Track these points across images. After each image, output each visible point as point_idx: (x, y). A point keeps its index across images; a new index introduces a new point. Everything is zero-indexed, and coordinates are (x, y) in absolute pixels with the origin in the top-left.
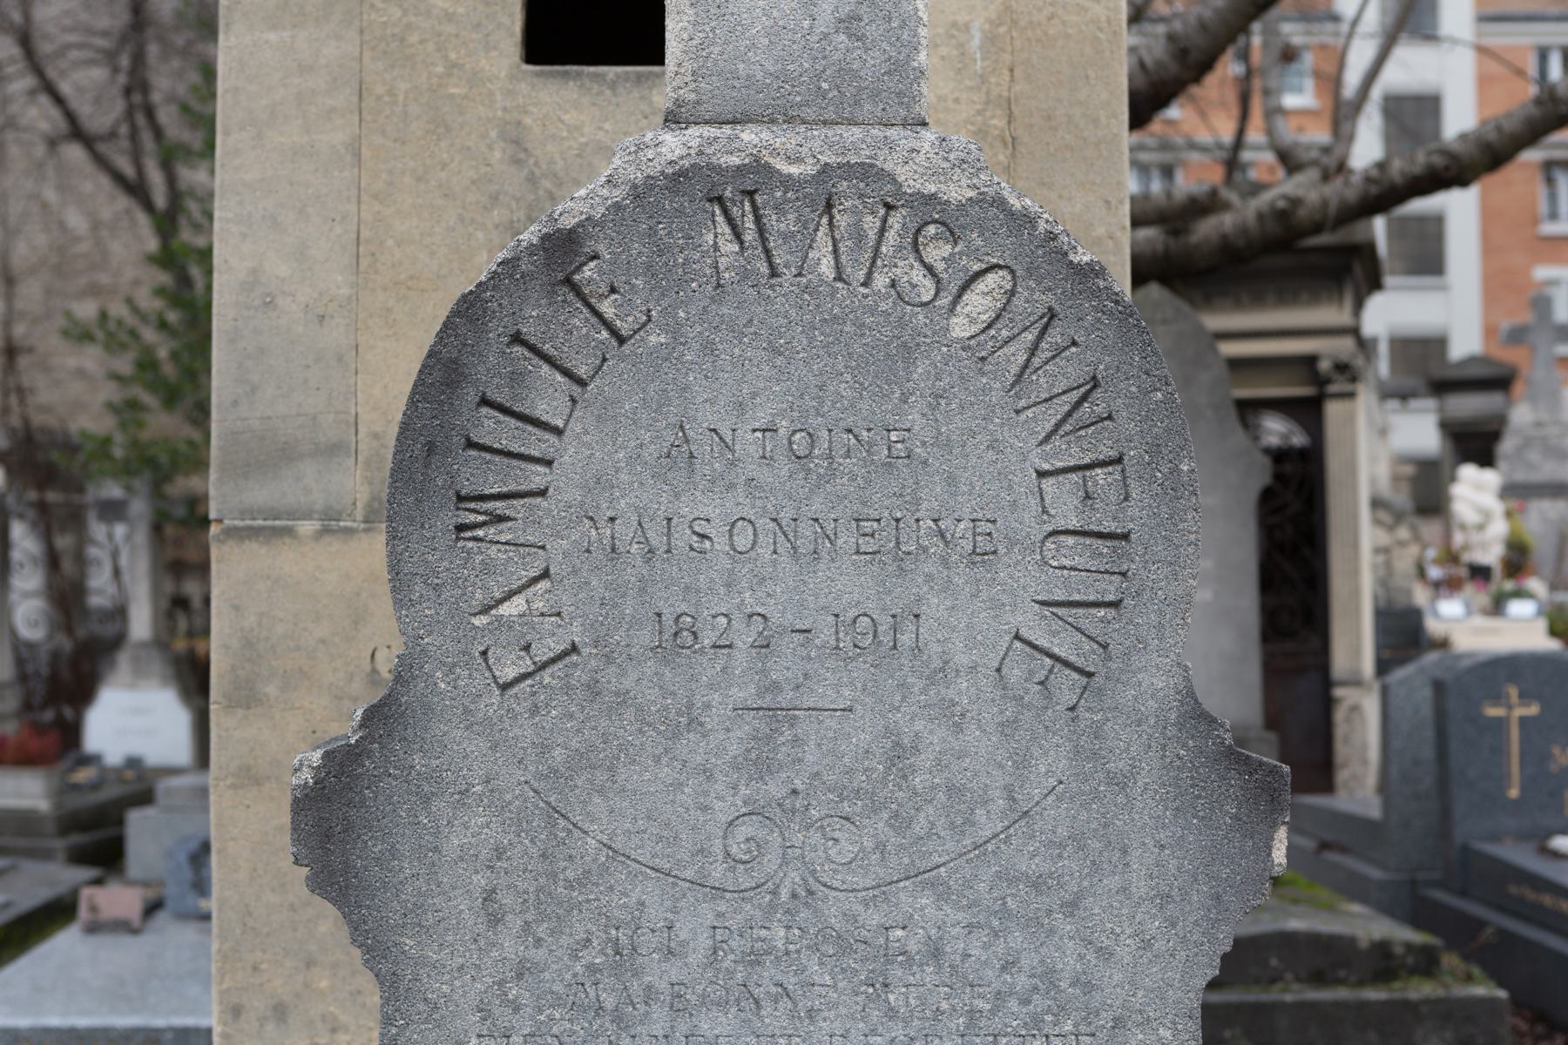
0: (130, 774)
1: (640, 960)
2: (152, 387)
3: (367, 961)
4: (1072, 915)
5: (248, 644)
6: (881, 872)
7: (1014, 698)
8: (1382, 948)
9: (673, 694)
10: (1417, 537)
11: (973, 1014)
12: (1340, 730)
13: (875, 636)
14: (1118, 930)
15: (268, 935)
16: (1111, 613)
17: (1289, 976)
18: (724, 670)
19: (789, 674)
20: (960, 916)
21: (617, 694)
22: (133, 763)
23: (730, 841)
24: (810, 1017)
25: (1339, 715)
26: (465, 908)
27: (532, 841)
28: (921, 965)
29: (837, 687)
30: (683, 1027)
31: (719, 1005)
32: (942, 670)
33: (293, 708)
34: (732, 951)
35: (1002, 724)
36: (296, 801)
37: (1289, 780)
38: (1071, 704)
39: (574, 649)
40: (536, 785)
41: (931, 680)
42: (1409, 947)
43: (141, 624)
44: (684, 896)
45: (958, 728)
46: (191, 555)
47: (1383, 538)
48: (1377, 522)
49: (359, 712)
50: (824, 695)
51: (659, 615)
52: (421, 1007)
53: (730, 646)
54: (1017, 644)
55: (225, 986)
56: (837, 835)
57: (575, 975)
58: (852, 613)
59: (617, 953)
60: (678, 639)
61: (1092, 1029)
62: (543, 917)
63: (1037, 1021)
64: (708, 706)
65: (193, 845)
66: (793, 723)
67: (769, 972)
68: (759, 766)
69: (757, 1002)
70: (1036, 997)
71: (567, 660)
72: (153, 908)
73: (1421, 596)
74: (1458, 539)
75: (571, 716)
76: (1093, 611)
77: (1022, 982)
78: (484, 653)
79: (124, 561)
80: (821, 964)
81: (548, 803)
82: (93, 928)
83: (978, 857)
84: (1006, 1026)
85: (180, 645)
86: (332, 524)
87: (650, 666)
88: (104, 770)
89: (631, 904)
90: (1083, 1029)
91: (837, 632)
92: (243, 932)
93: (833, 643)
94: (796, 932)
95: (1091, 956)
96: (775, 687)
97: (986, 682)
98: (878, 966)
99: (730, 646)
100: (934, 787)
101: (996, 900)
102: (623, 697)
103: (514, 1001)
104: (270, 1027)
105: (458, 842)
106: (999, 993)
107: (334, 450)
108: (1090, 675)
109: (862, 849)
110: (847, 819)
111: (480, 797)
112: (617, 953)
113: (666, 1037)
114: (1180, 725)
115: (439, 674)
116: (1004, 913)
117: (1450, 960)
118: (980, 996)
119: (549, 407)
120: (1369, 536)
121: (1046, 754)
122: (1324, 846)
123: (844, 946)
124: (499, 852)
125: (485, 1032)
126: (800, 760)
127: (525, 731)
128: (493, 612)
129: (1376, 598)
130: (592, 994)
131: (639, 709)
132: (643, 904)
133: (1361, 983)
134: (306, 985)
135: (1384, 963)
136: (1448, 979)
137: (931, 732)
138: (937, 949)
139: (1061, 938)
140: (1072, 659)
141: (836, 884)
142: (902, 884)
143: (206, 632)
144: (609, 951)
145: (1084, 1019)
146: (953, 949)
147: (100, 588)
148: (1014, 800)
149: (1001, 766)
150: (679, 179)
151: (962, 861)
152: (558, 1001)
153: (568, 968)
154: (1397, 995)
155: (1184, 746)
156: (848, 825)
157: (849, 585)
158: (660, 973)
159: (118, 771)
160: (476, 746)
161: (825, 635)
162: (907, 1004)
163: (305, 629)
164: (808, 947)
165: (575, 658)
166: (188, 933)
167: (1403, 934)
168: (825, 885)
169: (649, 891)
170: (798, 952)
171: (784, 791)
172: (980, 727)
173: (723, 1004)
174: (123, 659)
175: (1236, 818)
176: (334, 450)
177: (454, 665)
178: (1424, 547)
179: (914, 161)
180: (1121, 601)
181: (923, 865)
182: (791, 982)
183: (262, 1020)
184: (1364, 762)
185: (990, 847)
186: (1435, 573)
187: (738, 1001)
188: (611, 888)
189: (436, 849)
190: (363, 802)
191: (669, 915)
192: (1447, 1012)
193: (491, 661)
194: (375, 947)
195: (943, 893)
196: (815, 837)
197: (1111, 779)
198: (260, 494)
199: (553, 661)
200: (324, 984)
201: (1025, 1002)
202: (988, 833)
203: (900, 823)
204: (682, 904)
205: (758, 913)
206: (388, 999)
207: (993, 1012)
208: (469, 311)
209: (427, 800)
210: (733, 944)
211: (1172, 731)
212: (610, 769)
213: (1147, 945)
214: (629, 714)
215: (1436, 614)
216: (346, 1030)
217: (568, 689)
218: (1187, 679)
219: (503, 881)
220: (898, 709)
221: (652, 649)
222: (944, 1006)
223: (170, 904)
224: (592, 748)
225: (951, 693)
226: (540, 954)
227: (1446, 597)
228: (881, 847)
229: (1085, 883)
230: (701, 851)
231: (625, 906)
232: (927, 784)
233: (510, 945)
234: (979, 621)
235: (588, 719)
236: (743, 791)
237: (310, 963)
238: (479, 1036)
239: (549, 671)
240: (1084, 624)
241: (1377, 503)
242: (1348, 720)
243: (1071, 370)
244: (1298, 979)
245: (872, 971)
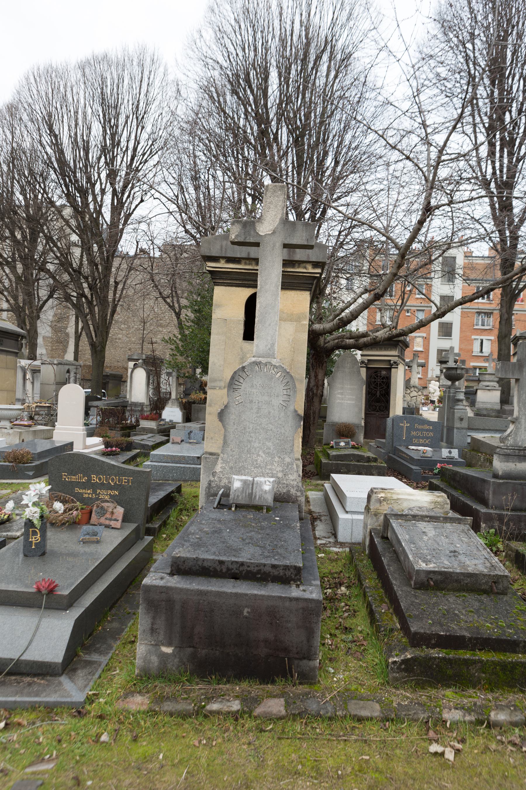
2: (178, 352)
8: (368, 457)
22: (171, 421)
26: (232, 423)
60: (251, 402)
82: (173, 443)
86: (220, 388)
105: (232, 417)
107: (221, 380)
119: (241, 381)
147: (164, 387)
150: (254, 362)
157: (266, 398)
158: (248, 430)
169: (247, 423)
176: (221, 380)
179: (274, 362)
194: (224, 426)
198: (213, 384)
208: (235, 373)
233: (235, 427)
234: (277, 402)
243: (286, 381)
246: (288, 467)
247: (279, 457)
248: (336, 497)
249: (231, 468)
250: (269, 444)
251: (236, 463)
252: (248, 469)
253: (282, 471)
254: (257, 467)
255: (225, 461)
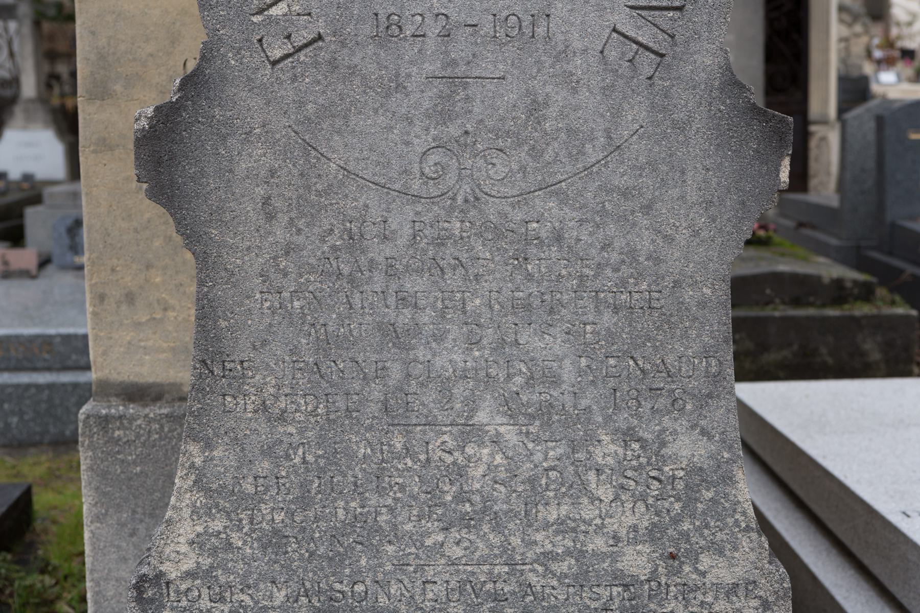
0: (26, 185)
1: (366, 242)
3: (187, 244)
4: (648, 214)
5: (102, 57)
6: (523, 185)
7: (612, 71)
8: (838, 283)
9: (386, 67)
10: (867, 32)
11: (582, 278)
12: (813, 152)
13: (520, 29)
14: (678, 224)
15: (121, 248)
16: (677, 14)
17: (777, 300)
18: (420, 51)
19: (463, 54)
20: (574, 214)
21: (349, 68)
22: (28, 177)
23: (424, 165)
24: (477, 280)
25: (813, 143)
26: (250, 210)
27: (294, 165)
28: (549, 246)
29: (495, 63)
30: (394, 286)
31: (417, 271)
32: (564, 52)
33: (132, 100)
34: (426, 237)
35: (603, 88)
36: (137, 140)
37: (792, 126)
38: (649, 75)
39: (320, 37)
40: (296, 128)
41: (557, 58)
42: (855, 282)
43: (29, 87)
44: (394, 201)
45: (575, 91)
46: (62, 46)
47: (845, 32)
48: (841, 21)
49: (178, 81)
50: (486, 69)
51: (376, 15)
52: (223, 274)
53: (423, 36)
54: (615, 35)
55: (93, 282)
56: (494, 161)
57: (323, 253)
58: (505, 13)
59: (351, 238)
61: (660, 288)
62: (302, 215)
63: (624, 282)
64: (409, 76)
65: (69, 222)
66: (465, 86)
67: (450, 250)
68: (443, 114)
69: (442, 270)
70: (623, 267)
71: (316, 45)
72: (44, 262)
73: (868, 69)
74: (894, 31)
75: (319, 82)
76: (666, 13)
77: (615, 257)
78: (260, 41)
79: (16, 47)
80: (484, 245)
81: (304, 140)
83: (587, 175)
84: (604, 286)
85: (56, 101)
87: (370, 50)
88: (9, 183)
89: (359, 206)
90: (653, 287)
91: (495, 27)
92: (104, 247)
93: (492, 33)
94: (468, 224)
95: (659, 241)
96: (454, 63)
97: (593, 59)
98: (521, 246)
99: (423, 36)
100: (558, 130)
101: (598, 204)
102: (353, 68)
103: (283, 270)
104: (124, 307)
105: (245, 165)
106: (599, 264)
108: (662, 56)
109: (511, 171)
110: (501, 150)
111: (259, 136)
112: (351, 238)
113: (383, 292)
114: (721, 89)
115: (230, 55)
116: (603, 212)
117: (881, 292)
118: (587, 266)
120: (836, 30)
121: (632, 108)
122: (801, 225)
123: (499, 235)
124: (272, 173)
125: (265, 290)
126: (470, 112)
127: (287, 93)
128: (266, 13)
129: (839, 70)
130: (334, 264)
131: (364, 78)
132: (367, 206)
133: (824, 305)
134: (147, 281)
135: (838, 293)
136: (880, 303)
137: (557, 93)
138: (559, 236)
139: (640, 229)
140: (651, 45)
141: (494, 193)
142: (537, 193)
143: (71, 55)
144: (346, 237)
145: (655, 281)
146: (570, 235)
148: (611, 138)
149: (602, 116)
151: (576, 178)
152: (312, 270)
153: (319, 248)
154: (847, 313)
155: (724, 103)
156: (502, 154)
158: (378, 252)
159: (17, 183)
160: (256, 102)
161: (487, 28)
162: (540, 271)
163: (139, 47)
164: (475, 234)
165: (320, 43)
166: (68, 278)
167: (851, 275)
168: (486, 194)
169: (371, 198)
170: (469, 237)
171: (460, 132)
172: (589, 90)
173: (419, 271)
174: (18, 111)
175: (757, 151)
177: (240, 49)
178: (872, 37)
180: (684, 6)
181: (551, 181)
182: (464, 257)
183: (119, 303)
184: (829, 174)
185: (595, 169)
186: (878, 54)
187: (429, 269)
188: (346, 196)
189: (231, 171)
190: (182, 140)
191: (385, 214)
192: (879, 324)
193: (265, 46)
194: (192, 236)
195: (563, 199)
196: (480, 162)
197: (675, 125)
199: (306, 46)
200: (158, 280)
201: (616, 270)
202: (594, 160)
203: (536, 153)
204: (393, 206)
205: (443, 212)
206: (201, 269)
207: (596, 276)
209: (224, 138)
210: (427, 232)
211: (715, 93)
212: (344, 118)
213: (696, 234)
214: (357, 81)
215: (878, 81)
216: (174, 309)
217: (316, 64)
218: (726, 59)
219: (275, 192)
220: (535, 78)
221: (372, 38)
222: (564, 272)
223: (55, 260)
224: (333, 103)
225: (570, 67)
226: (300, 239)
227: (884, 70)
228: (523, 169)
229: (657, 193)
230: (405, 171)
231: (356, 207)
232: (554, 128)
233: (280, 234)
235: (330, 84)
236: (433, 132)
237: (149, 266)
238: (261, 292)
239: (303, 52)
240: (659, 21)
241: (842, 9)
242: (818, 146)
244: (784, 303)
245: (517, 250)
246: (690, 498)
247: (628, 436)
248: (822, 543)
249: (274, 541)
250: (548, 345)
251: (304, 501)
252: (396, 536)
253: (654, 534)
254: (466, 522)
255: (215, 495)
